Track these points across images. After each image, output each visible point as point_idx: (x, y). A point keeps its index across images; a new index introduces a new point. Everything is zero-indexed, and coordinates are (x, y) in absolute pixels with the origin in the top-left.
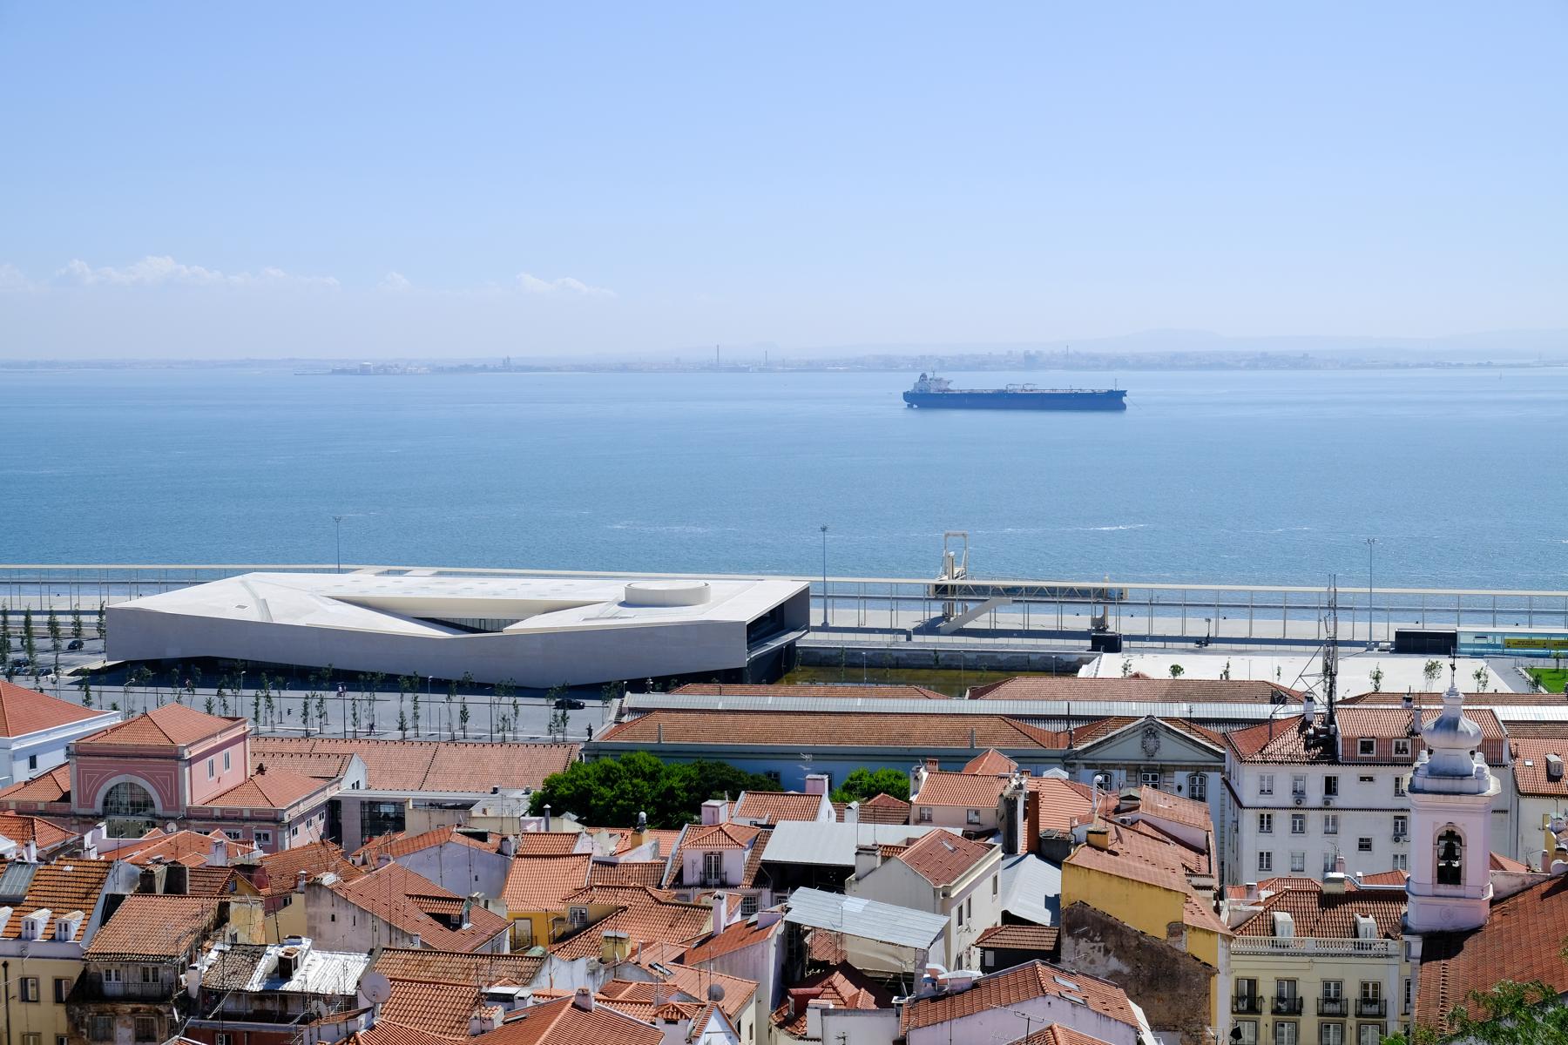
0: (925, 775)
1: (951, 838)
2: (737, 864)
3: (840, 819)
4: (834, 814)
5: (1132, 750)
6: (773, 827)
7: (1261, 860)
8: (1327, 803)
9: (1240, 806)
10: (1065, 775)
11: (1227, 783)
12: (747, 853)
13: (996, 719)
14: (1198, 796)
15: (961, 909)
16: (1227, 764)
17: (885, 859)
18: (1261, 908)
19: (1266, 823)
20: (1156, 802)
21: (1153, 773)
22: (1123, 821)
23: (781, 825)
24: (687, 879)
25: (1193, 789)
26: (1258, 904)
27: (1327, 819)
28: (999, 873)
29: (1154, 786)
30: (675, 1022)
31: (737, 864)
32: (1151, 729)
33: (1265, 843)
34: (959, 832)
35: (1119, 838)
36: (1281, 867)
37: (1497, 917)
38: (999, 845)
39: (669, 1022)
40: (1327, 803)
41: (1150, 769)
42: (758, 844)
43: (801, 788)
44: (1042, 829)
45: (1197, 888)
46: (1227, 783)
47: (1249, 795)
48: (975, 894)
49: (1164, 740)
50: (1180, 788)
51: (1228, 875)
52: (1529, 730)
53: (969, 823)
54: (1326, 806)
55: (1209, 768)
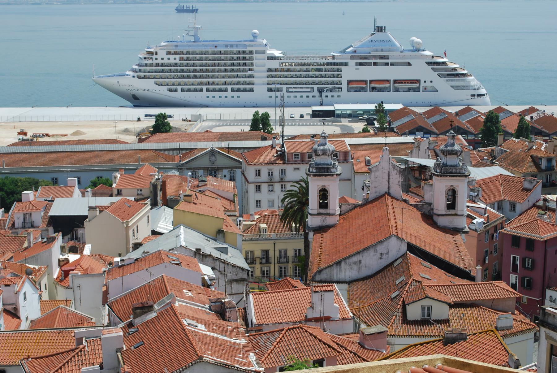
0: (119, 176)
1: (129, 201)
2: (38, 218)
3: (83, 196)
4: (81, 194)
5: (205, 162)
6: (53, 201)
7: (257, 203)
8: (271, 179)
9: (248, 182)
10: (177, 173)
11: (243, 174)
12: (42, 213)
13: (149, 151)
14: (232, 179)
15: (134, 230)
16: (243, 166)
17: (101, 212)
18: (254, 223)
19: (258, 189)
20: (212, 181)
21: (214, 171)
22: (200, 191)
23: (57, 200)
24: (16, 226)
25: (231, 176)
26: (253, 221)
27: (282, 185)
28: (150, 214)
29: (215, 176)
30: (9, 285)
31: (38, 218)
32: (213, 152)
33: (258, 196)
34: (132, 199)
35: (197, 198)
36: (265, 205)
37: (342, 221)
38: (149, 203)
39: (6, 285)
40: (282, 179)
41: (213, 169)
42: (47, 208)
43: (66, 184)
44: (168, 197)
45: (229, 216)
46: (243, 174)
47: (251, 176)
48: (139, 224)
49: (219, 157)
50: (225, 176)
51: (243, 212)
52: (375, 146)
53: (138, 194)
54: (282, 180)
55: (237, 168)
